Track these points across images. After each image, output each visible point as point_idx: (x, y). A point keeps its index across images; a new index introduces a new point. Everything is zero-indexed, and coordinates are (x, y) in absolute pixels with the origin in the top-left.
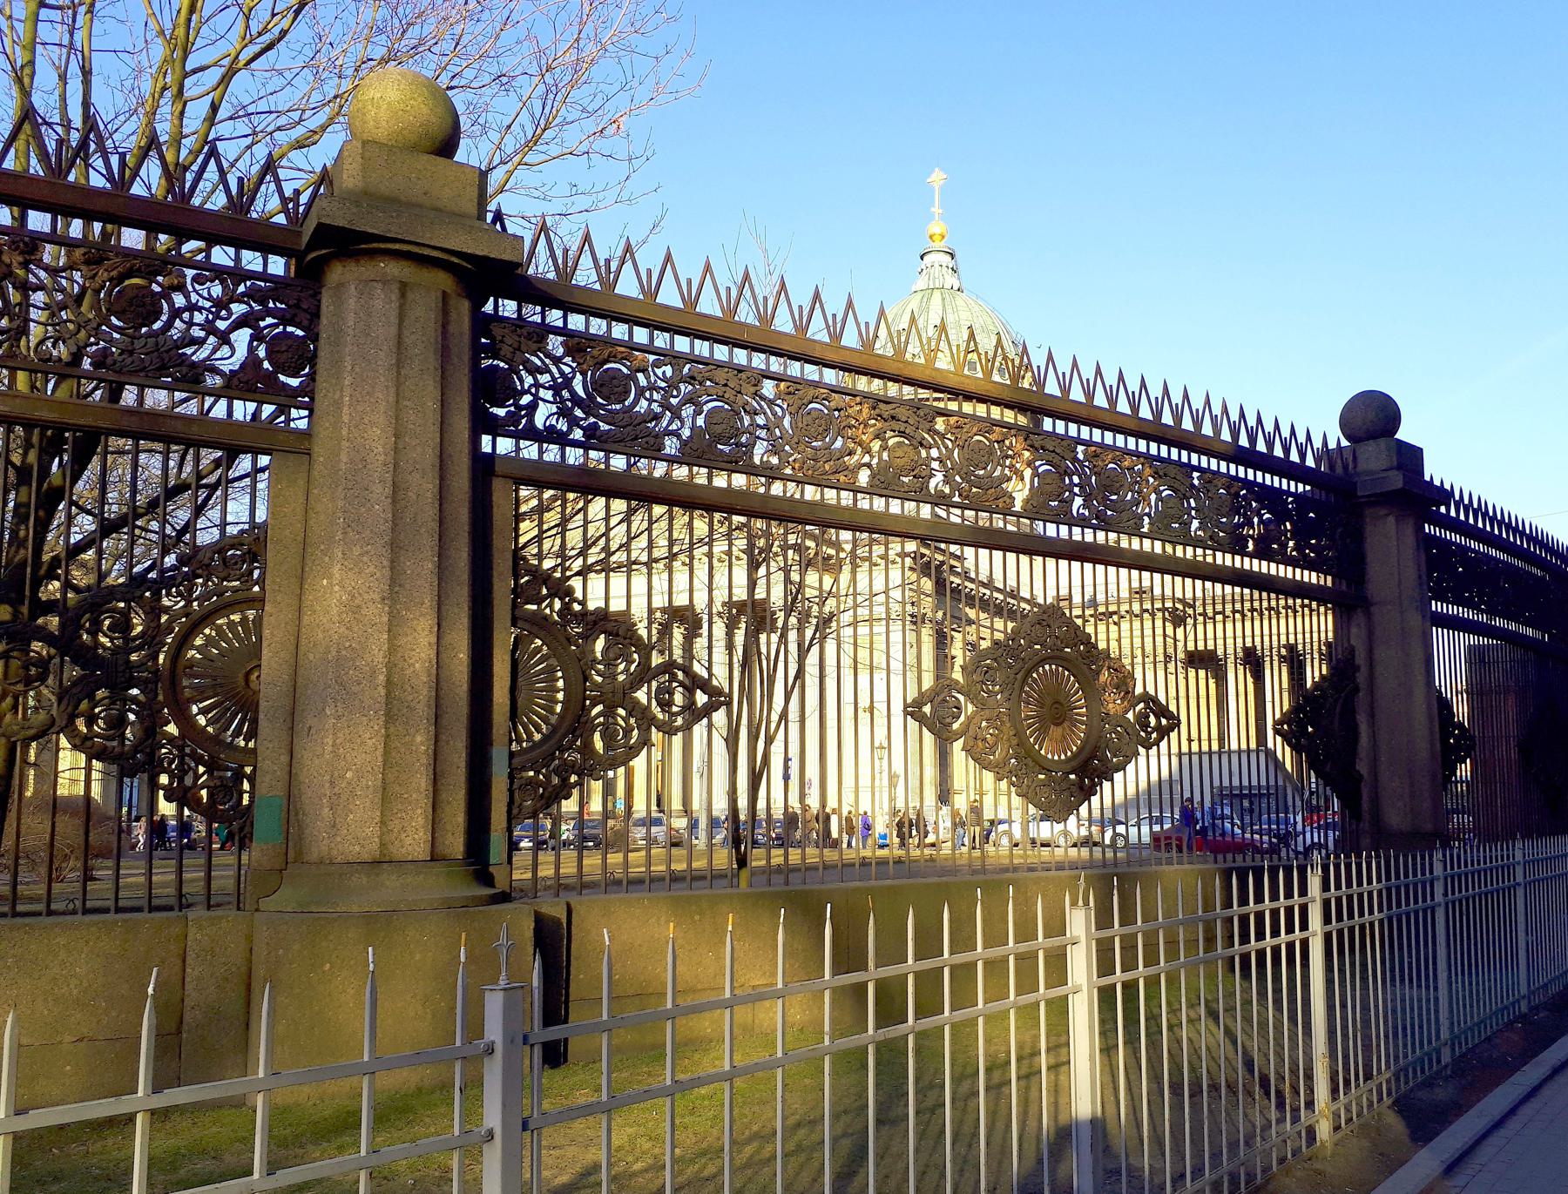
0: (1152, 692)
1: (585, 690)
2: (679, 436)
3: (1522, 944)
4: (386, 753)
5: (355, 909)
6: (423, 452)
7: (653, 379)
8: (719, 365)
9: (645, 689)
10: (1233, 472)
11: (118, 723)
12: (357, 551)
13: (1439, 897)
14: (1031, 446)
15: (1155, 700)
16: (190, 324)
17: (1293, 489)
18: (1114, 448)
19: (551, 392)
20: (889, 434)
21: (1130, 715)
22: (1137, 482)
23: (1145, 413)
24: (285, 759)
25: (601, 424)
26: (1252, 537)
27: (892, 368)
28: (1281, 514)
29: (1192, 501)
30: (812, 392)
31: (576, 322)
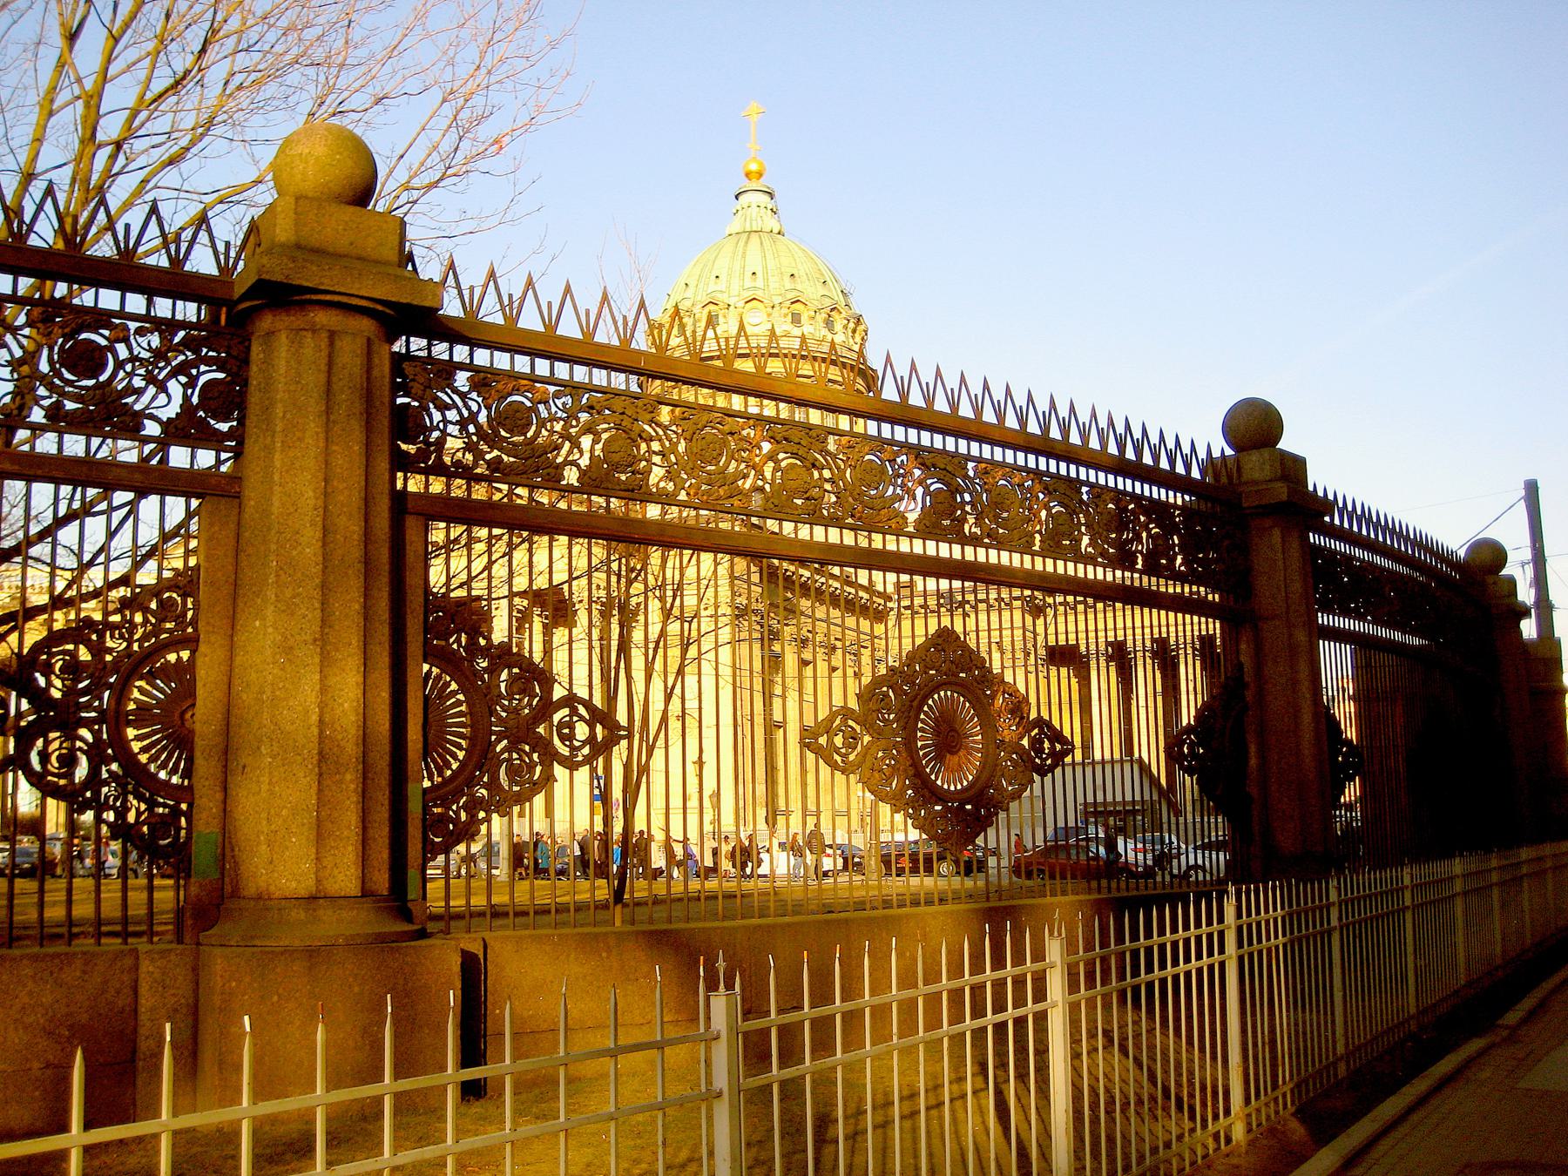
0: (1046, 717)
3: (1411, 965)
4: (320, 791)
5: (297, 943)
6: (349, 495)
7: (554, 409)
8: (617, 394)
10: (1120, 486)
11: (69, 761)
12: (288, 593)
13: (1334, 922)
14: (923, 464)
15: (1049, 725)
16: (131, 375)
17: (1179, 502)
18: (1003, 464)
20: (781, 456)
21: (1025, 742)
22: (1027, 499)
23: (1033, 428)
24: (219, 796)
25: (504, 456)
27: (784, 390)
28: (1168, 528)
30: (705, 417)
31: (482, 357)
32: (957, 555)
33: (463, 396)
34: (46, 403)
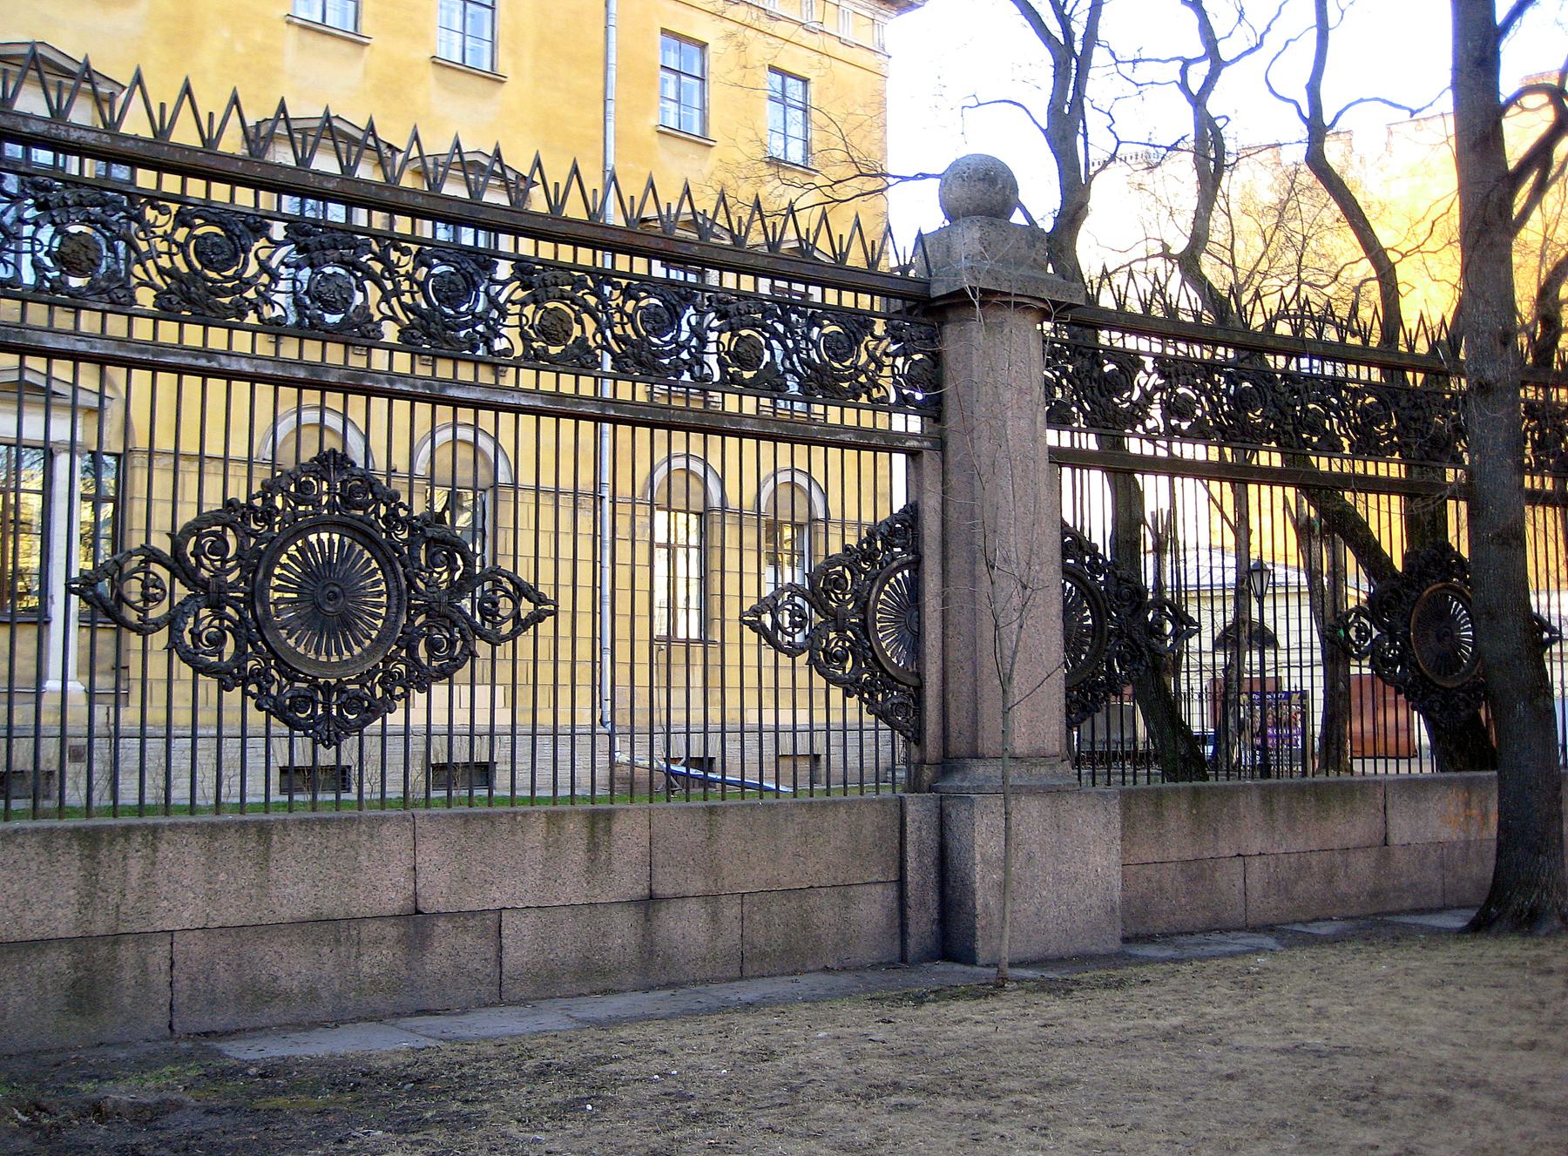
1: (410, 599)
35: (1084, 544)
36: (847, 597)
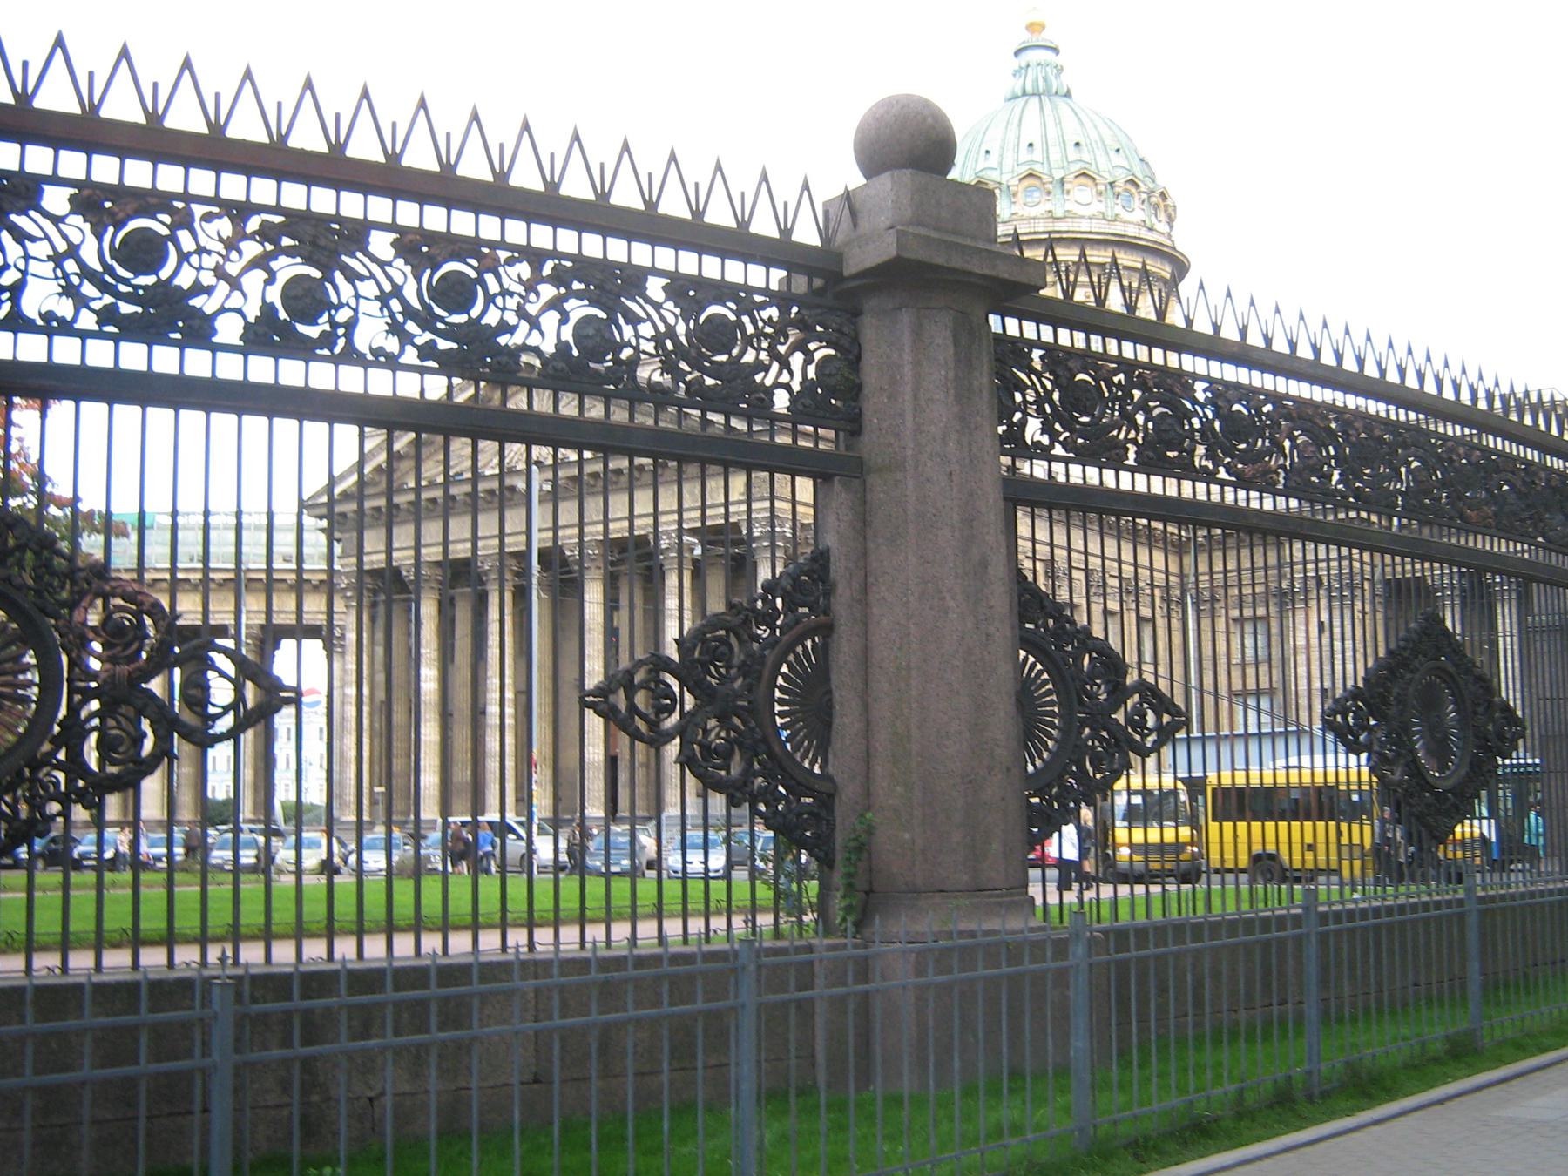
0: (1151, 679)
2: (787, 387)
9: (1122, 709)
19: (653, 344)
26: (1401, 493)
29: (1331, 448)
32: (1172, 491)
33: (57, 220)
34: (97, 305)
35: (1046, 603)
36: (733, 672)
